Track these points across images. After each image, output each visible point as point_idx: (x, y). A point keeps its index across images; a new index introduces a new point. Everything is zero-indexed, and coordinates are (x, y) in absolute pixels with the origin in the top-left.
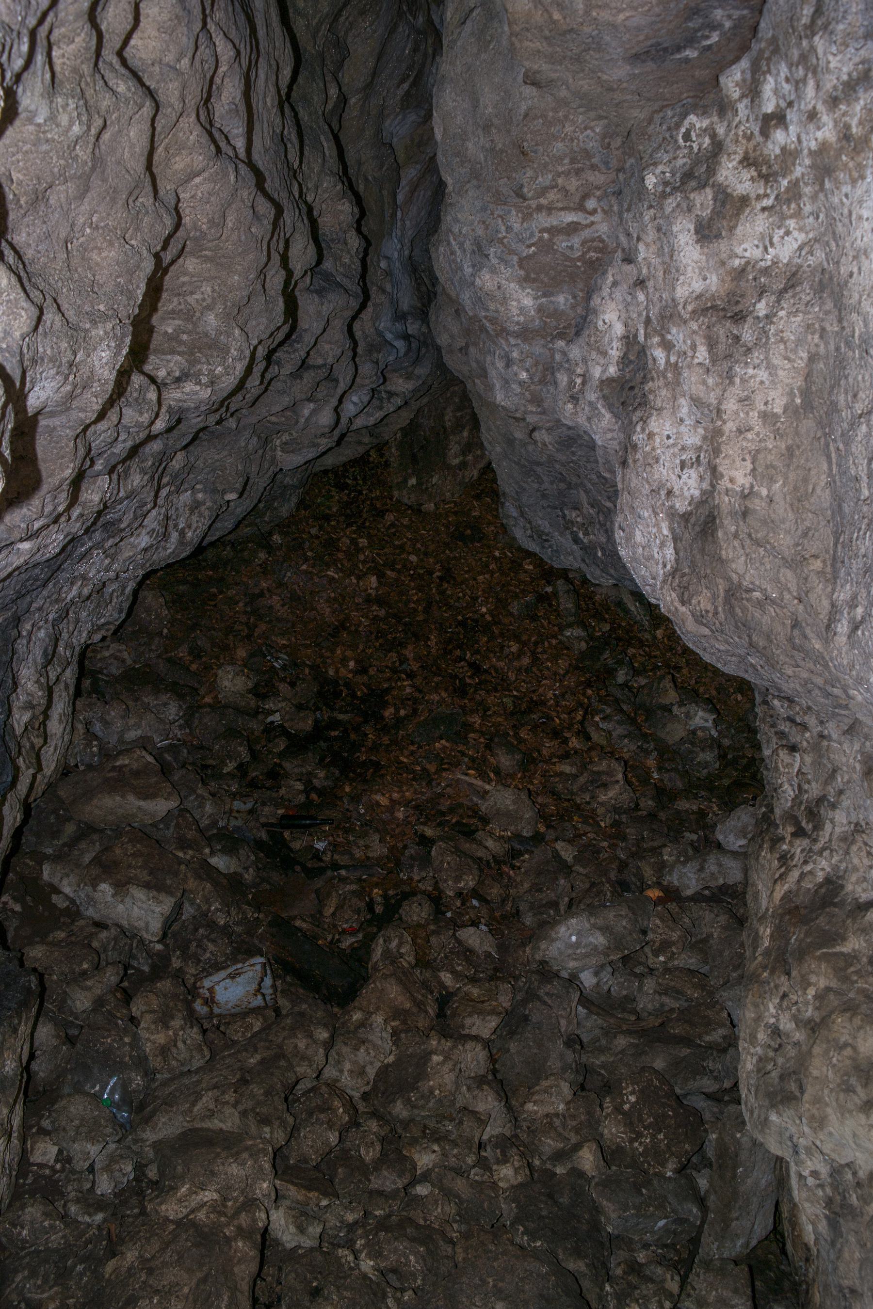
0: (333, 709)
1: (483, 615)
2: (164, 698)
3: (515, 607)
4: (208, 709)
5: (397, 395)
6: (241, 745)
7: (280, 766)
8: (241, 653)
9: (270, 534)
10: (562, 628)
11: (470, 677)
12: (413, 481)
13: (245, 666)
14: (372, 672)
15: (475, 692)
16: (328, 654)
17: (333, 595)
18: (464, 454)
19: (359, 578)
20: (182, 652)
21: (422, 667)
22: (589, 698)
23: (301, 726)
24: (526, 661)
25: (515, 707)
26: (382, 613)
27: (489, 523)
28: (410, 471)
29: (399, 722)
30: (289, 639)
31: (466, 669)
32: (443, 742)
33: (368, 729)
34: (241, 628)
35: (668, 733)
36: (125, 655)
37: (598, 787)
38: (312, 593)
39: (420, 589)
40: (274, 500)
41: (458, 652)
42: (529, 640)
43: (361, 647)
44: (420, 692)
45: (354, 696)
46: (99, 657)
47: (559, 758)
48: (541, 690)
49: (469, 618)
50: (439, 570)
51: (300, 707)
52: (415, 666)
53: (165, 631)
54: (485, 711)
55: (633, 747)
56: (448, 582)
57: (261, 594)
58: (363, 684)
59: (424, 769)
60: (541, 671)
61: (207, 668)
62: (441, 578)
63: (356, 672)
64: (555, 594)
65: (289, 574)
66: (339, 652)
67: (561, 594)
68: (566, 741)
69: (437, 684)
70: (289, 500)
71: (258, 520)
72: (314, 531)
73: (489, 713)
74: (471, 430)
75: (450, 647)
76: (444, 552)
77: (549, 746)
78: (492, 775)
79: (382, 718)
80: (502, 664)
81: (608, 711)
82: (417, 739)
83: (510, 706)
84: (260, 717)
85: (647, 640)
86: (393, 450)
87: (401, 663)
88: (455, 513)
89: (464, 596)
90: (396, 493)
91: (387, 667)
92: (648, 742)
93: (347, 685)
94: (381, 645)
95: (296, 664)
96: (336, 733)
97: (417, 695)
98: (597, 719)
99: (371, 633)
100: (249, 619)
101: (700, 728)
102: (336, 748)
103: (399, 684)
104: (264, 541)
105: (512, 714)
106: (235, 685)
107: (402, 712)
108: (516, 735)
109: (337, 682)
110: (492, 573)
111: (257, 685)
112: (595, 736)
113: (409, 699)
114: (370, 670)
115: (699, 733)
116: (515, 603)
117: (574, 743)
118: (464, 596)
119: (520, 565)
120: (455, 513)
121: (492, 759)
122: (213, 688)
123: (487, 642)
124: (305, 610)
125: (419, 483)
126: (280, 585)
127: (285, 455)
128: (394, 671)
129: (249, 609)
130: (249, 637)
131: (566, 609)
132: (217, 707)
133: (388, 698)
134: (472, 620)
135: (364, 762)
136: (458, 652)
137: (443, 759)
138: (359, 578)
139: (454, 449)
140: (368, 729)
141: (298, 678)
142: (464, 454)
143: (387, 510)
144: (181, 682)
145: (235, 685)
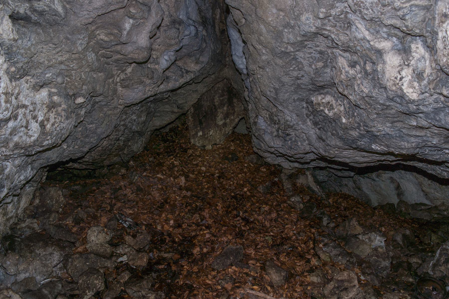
0: (160, 251)
1: (245, 192)
2: (50, 250)
3: (261, 189)
4: (77, 256)
5: (191, 72)
6: (96, 279)
7: (125, 292)
8: (104, 219)
9: (128, 162)
10: (289, 197)
11: (244, 226)
12: (200, 133)
13: (106, 227)
14: (184, 226)
15: (248, 235)
16: (157, 217)
17: (160, 187)
18: (225, 119)
19: (175, 178)
20: (69, 221)
21: (214, 221)
22: (314, 234)
23: (139, 263)
24: (274, 215)
25: (273, 242)
26: (189, 194)
27: (240, 152)
28: (199, 128)
29: (204, 256)
30: (134, 210)
31: (241, 221)
32: (234, 267)
33: (183, 262)
34: (106, 206)
35: (361, 251)
36: (36, 226)
37: (342, 291)
38: (149, 186)
39: (208, 182)
40: (129, 141)
41: (235, 212)
42: (273, 204)
43: (177, 213)
44: (215, 236)
45: (174, 242)
46: (18, 227)
47: (307, 272)
48: (286, 231)
49: (238, 194)
50: (218, 173)
51: (139, 251)
52: (210, 222)
53: (61, 210)
54: (256, 246)
55: (344, 262)
56: (223, 178)
57: (120, 188)
58: (180, 234)
59: (223, 288)
60: (283, 220)
61: (82, 229)
62: (219, 177)
63: (174, 227)
64: (281, 181)
65: (136, 178)
66: (164, 215)
67: (284, 181)
68: (308, 261)
69: (225, 231)
70: (137, 142)
71: (120, 153)
72: (151, 159)
73: (258, 247)
74: (228, 107)
75: (230, 209)
76: (219, 165)
77: (300, 266)
78: (269, 288)
79: (192, 254)
80: (260, 217)
81: (326, 241)
82: (216, 267)
83: (270, 242)
84: (114, 259)
85: (326, 204)
86: (190, 118)
87: (202, 220)
88: (223, 148)
89: (234, 183)
90: (192, 141)
91: (193, 223)
92: (352, 258)
93: (169, 235)
94: (189, 210)
95: (137, 224)
96: (163, 266)
97: (213, 238)
98: (321, 245)
99: (183, 204)
100: (112, 201)
101: (379, 247)
102: (163, 277)
103: (201, 232)
104: (125, 165)
105: (273, 246)
106: (98, 239)
107: (205, 250)
108: (278, 259)
109: (163, 233)
110: (246, 173)
111: (113, 238)
112: (322, 256)
113: (209, 241)
114: (183, 225)
115: (380, 250)
116: (261, 186)
117: (314, 262)
118: (234, 183)
119: (259, 170)
120: (223, 148)
121: (267, 277)
122: (85, 241)
123: (251, 206)
124: (145, 195)
125: (204, 134)
126: (131, 183)
127: (124, 90)
128: (198, 225)
129: (113, 197)
130: (110, 211)
131: (287, 188)
132: (85, 253)
133: (196, 241)
134: (240, 195)
135: (181, 286)
136: (235, 212)
137: (235, 279)
138: (175, 178)
139: (220, 116)
140: (183, 262)
141: (138, 232)
142: (225, 119)
143: (188, 148)
144: (64, 239)
145: (98, 239)
